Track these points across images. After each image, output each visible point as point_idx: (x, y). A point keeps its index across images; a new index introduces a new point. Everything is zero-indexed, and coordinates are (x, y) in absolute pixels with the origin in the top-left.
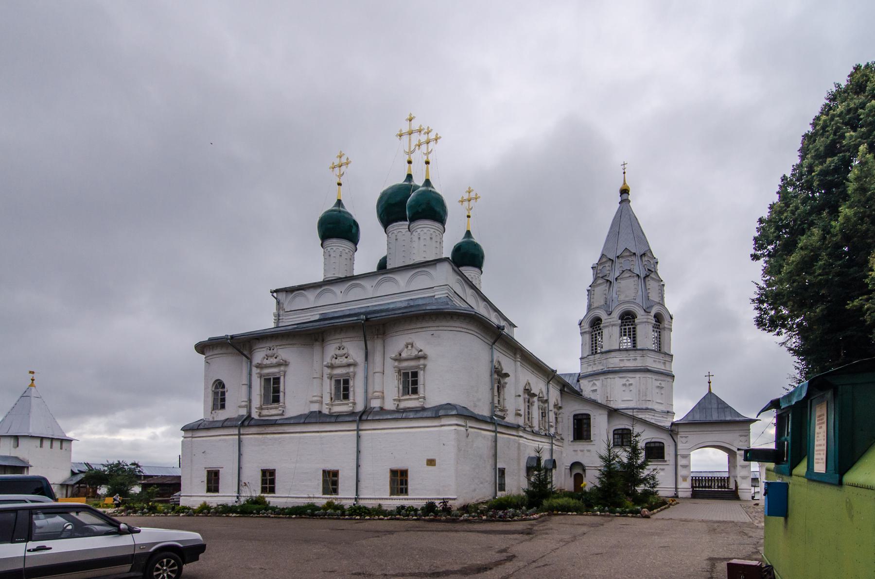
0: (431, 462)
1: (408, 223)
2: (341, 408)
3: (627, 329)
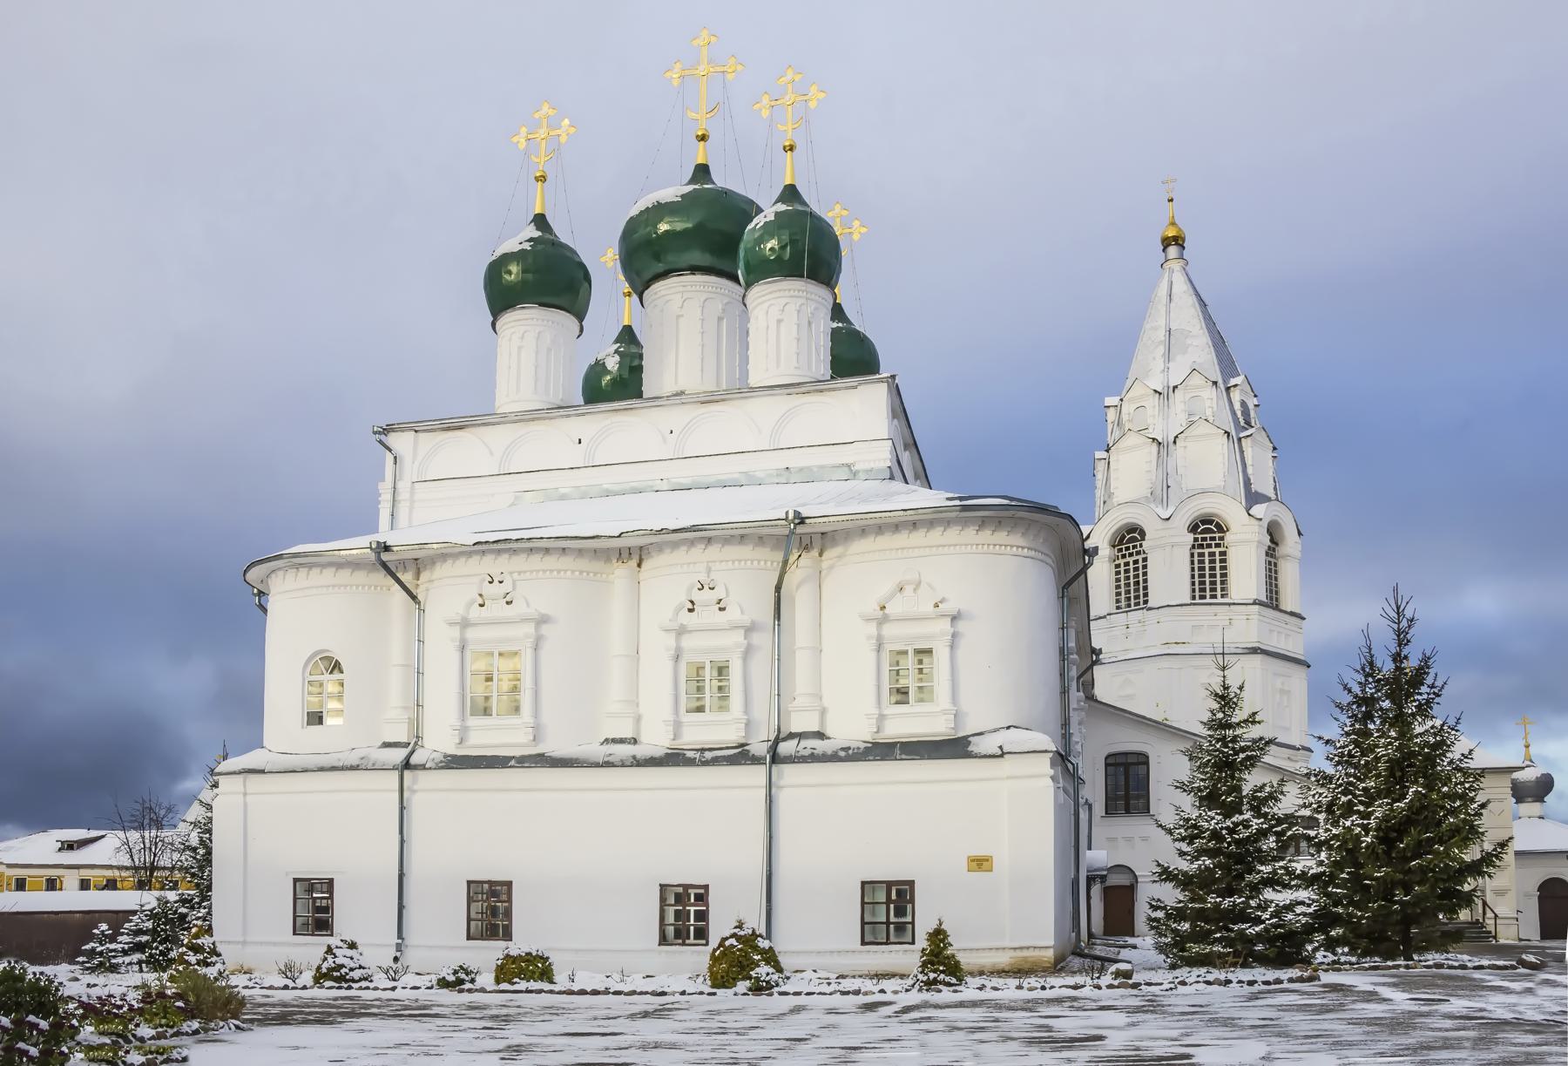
0: (980, 863)
3: (1207, 555)
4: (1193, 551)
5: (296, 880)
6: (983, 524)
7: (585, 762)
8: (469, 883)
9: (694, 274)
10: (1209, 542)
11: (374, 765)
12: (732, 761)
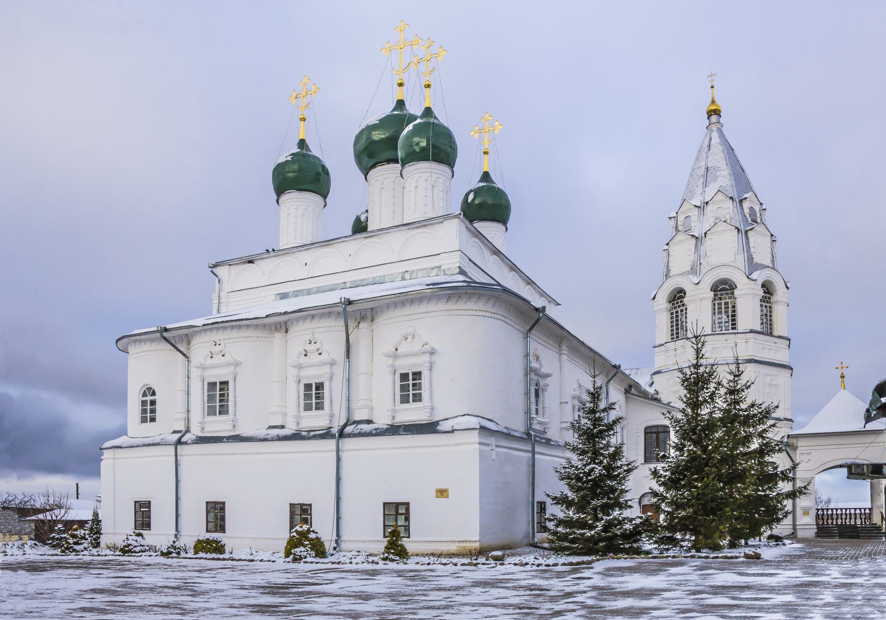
0: (442, 493)
1: (399, 166)
2: (316, 420)
4: (714, 302)
5: (135, 502)
6: (449, 298)
7: (256, 439)
8: (207, 503)
9: (389, 164)
10: (727, 296)
11: (166, 442)
12: (322, 437)
